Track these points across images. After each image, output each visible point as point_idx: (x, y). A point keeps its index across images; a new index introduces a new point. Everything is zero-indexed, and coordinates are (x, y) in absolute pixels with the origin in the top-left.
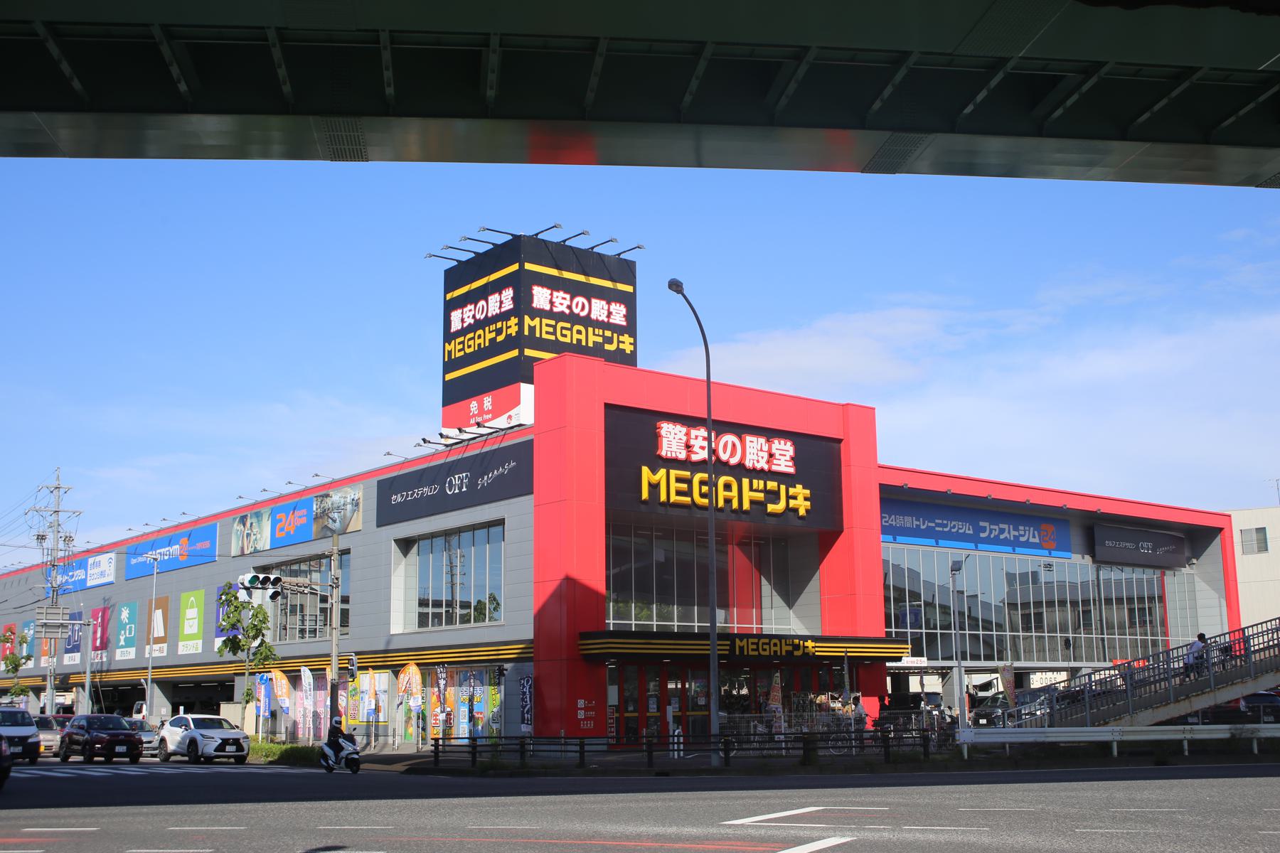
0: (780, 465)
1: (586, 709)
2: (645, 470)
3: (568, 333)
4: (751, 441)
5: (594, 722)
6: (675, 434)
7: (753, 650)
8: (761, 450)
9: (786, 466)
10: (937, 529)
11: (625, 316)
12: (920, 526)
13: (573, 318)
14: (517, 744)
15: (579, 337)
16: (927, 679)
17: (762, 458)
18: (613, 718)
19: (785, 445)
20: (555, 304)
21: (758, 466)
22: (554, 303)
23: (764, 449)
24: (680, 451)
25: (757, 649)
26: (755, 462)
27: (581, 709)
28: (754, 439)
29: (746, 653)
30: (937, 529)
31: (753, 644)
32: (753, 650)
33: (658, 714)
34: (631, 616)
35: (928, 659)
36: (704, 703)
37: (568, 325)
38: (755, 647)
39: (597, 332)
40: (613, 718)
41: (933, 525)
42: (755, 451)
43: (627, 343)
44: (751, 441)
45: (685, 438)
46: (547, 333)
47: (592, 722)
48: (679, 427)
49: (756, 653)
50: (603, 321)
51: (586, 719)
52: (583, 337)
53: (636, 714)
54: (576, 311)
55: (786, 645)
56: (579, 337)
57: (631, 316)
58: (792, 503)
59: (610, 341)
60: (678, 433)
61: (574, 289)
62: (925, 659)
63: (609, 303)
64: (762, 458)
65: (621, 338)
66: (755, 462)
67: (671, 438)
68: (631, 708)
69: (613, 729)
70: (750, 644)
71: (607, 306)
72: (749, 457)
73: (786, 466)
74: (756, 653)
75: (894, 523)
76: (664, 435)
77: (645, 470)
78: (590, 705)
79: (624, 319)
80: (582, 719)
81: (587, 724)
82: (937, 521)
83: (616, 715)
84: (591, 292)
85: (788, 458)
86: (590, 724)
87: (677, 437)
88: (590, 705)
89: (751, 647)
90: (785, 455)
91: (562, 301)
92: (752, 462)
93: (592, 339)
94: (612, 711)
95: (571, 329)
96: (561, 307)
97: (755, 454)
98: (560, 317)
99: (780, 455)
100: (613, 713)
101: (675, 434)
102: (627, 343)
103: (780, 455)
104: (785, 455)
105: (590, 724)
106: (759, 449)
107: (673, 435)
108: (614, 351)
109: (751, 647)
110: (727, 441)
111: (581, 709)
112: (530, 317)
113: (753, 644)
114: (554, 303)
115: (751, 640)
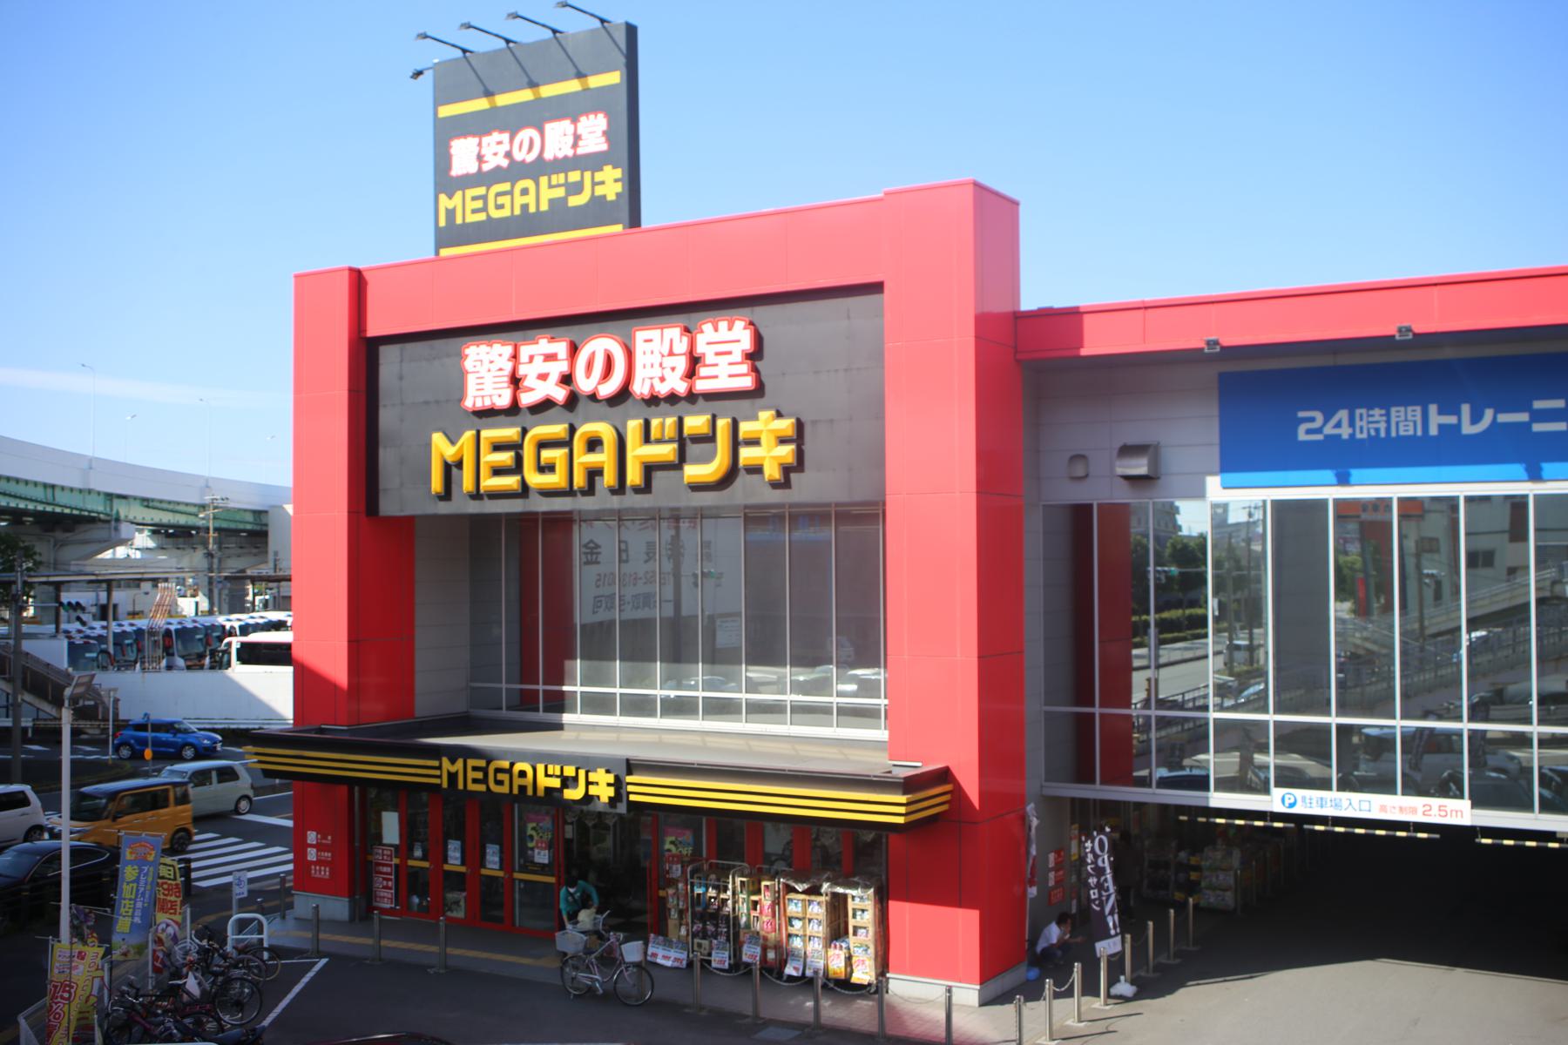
0: (716, 377)
1: (319, 847)
2: (438, 439)
3: (505, 200)
4: (647, 341)
5: (330, 869)
6: (491, 362)
7: (475, 781)
8: (671, 354)
9: (731, 376)
10: (1538, 427)
11: (604, 133)
12: (1458, 426)
13: (514, 171)
14: (275, 884)
15: (525, 200)
16: (137, 907)
17: (673, 369)
18: (390, 866)
19: (716, 329)
20: (485, 159)
21: (663, 389)
22: (483, 156)
23: (676, 350)
24: (500, 392)
25: (485, 781)
26: (657, 382)
27: (312, 846)
28: (654, 334)
29: (461, 786)
30: (1538, 427)
31: (475, 769)
32: (475, 781)
33: (501, 874)
34: (616, 683)
35: (1474, 806)
36: (546, 861)
37: (506, 187)
38: (480, 775)
39: (554, 182)
40: (390, 866)
41: (1523, 417)
42: (657, 359)
43: (609, 182)
44: (647, 341)
45: (508, 366)
46: (474, 211)
47: (327, 869)
48: (497, 347)
49: (482, 788)
50: (566, 157)
51: (319, 862)
52: (530, 199)
53: (426, 864)
54: (519, 156)
55: (547, 775)
56: (525, 200)
57: (443, 160)
58: (746, 454)
59: (577, 188)
60: (496, 358)
61: (510, 120)
62: (1465, 804)
63: (575, 121)
64: (673, 369)
65: (599, 176)
66: (657, 382)
67: (483, 371)
68: (418, 853)
69: (390, 883)
70: (469, 769)
71: (572, 126)
72: (640, 373)
73: (731, 376)
74: (482, 788)
75: (1345, 432)
76: (470, 370)
77: (438, 439)
78: (324, 841)
79: (603, 139)
80: (312, 862)
81: (320, 871)
82: (1539, 405)
83: (396, 861)
84: (537, 115)
85: (737, 356)
86: (325, 871)
87: (494, 367)
88: (324, 841)
89: (471, 775)
90: (729, 353)
91: (495, 149)
92: (648, 383)
93: (548, 194)
94: (389, 853)
95: (511, 193)
96: (495, 160)
97: (657, 366)
98: (497, 175)
99: (718, 354)
100: (391, 856)
101: (491, 362)
102: (609, 182)
103: (718, 354)
104: (729, 353)
105: (325, 871)
106: (666, 352)
107: (487, 365)
108: (587, 205)
109: (471, 775)
110: (594, 353)
111: (312, 846)
112: (447, 195)
113: (475, 769)
114: (483, 156)
115: (471, 763)
